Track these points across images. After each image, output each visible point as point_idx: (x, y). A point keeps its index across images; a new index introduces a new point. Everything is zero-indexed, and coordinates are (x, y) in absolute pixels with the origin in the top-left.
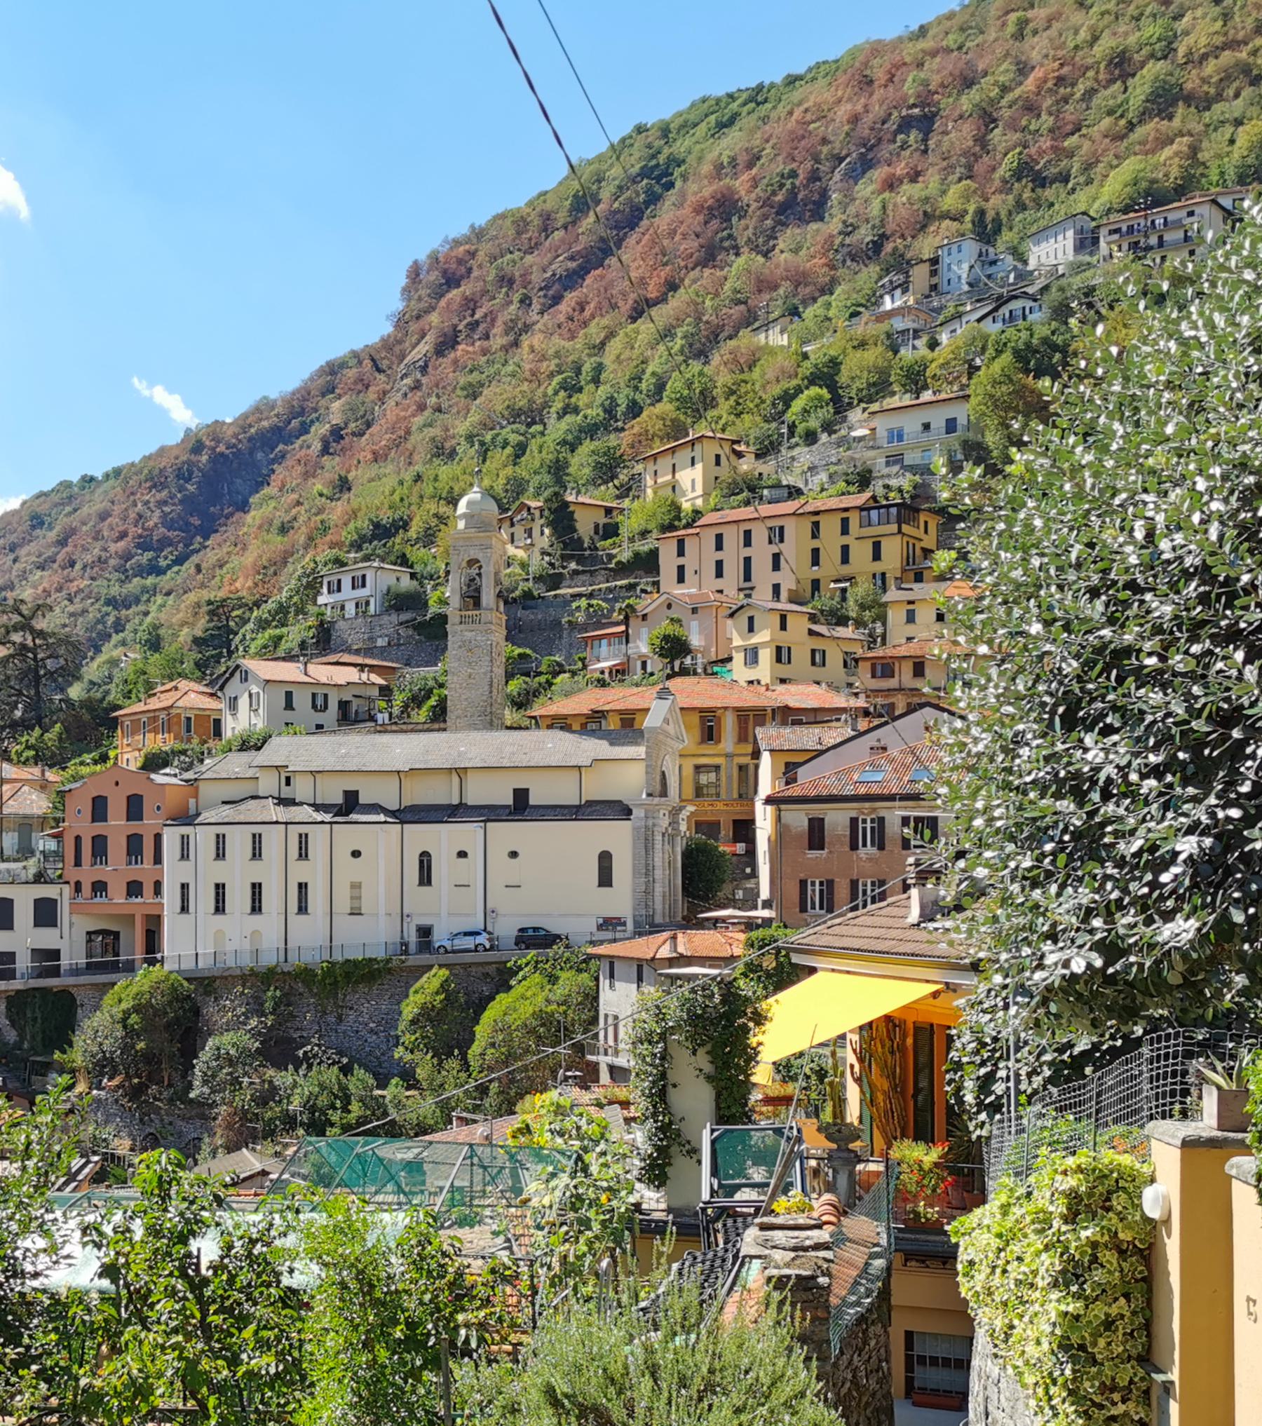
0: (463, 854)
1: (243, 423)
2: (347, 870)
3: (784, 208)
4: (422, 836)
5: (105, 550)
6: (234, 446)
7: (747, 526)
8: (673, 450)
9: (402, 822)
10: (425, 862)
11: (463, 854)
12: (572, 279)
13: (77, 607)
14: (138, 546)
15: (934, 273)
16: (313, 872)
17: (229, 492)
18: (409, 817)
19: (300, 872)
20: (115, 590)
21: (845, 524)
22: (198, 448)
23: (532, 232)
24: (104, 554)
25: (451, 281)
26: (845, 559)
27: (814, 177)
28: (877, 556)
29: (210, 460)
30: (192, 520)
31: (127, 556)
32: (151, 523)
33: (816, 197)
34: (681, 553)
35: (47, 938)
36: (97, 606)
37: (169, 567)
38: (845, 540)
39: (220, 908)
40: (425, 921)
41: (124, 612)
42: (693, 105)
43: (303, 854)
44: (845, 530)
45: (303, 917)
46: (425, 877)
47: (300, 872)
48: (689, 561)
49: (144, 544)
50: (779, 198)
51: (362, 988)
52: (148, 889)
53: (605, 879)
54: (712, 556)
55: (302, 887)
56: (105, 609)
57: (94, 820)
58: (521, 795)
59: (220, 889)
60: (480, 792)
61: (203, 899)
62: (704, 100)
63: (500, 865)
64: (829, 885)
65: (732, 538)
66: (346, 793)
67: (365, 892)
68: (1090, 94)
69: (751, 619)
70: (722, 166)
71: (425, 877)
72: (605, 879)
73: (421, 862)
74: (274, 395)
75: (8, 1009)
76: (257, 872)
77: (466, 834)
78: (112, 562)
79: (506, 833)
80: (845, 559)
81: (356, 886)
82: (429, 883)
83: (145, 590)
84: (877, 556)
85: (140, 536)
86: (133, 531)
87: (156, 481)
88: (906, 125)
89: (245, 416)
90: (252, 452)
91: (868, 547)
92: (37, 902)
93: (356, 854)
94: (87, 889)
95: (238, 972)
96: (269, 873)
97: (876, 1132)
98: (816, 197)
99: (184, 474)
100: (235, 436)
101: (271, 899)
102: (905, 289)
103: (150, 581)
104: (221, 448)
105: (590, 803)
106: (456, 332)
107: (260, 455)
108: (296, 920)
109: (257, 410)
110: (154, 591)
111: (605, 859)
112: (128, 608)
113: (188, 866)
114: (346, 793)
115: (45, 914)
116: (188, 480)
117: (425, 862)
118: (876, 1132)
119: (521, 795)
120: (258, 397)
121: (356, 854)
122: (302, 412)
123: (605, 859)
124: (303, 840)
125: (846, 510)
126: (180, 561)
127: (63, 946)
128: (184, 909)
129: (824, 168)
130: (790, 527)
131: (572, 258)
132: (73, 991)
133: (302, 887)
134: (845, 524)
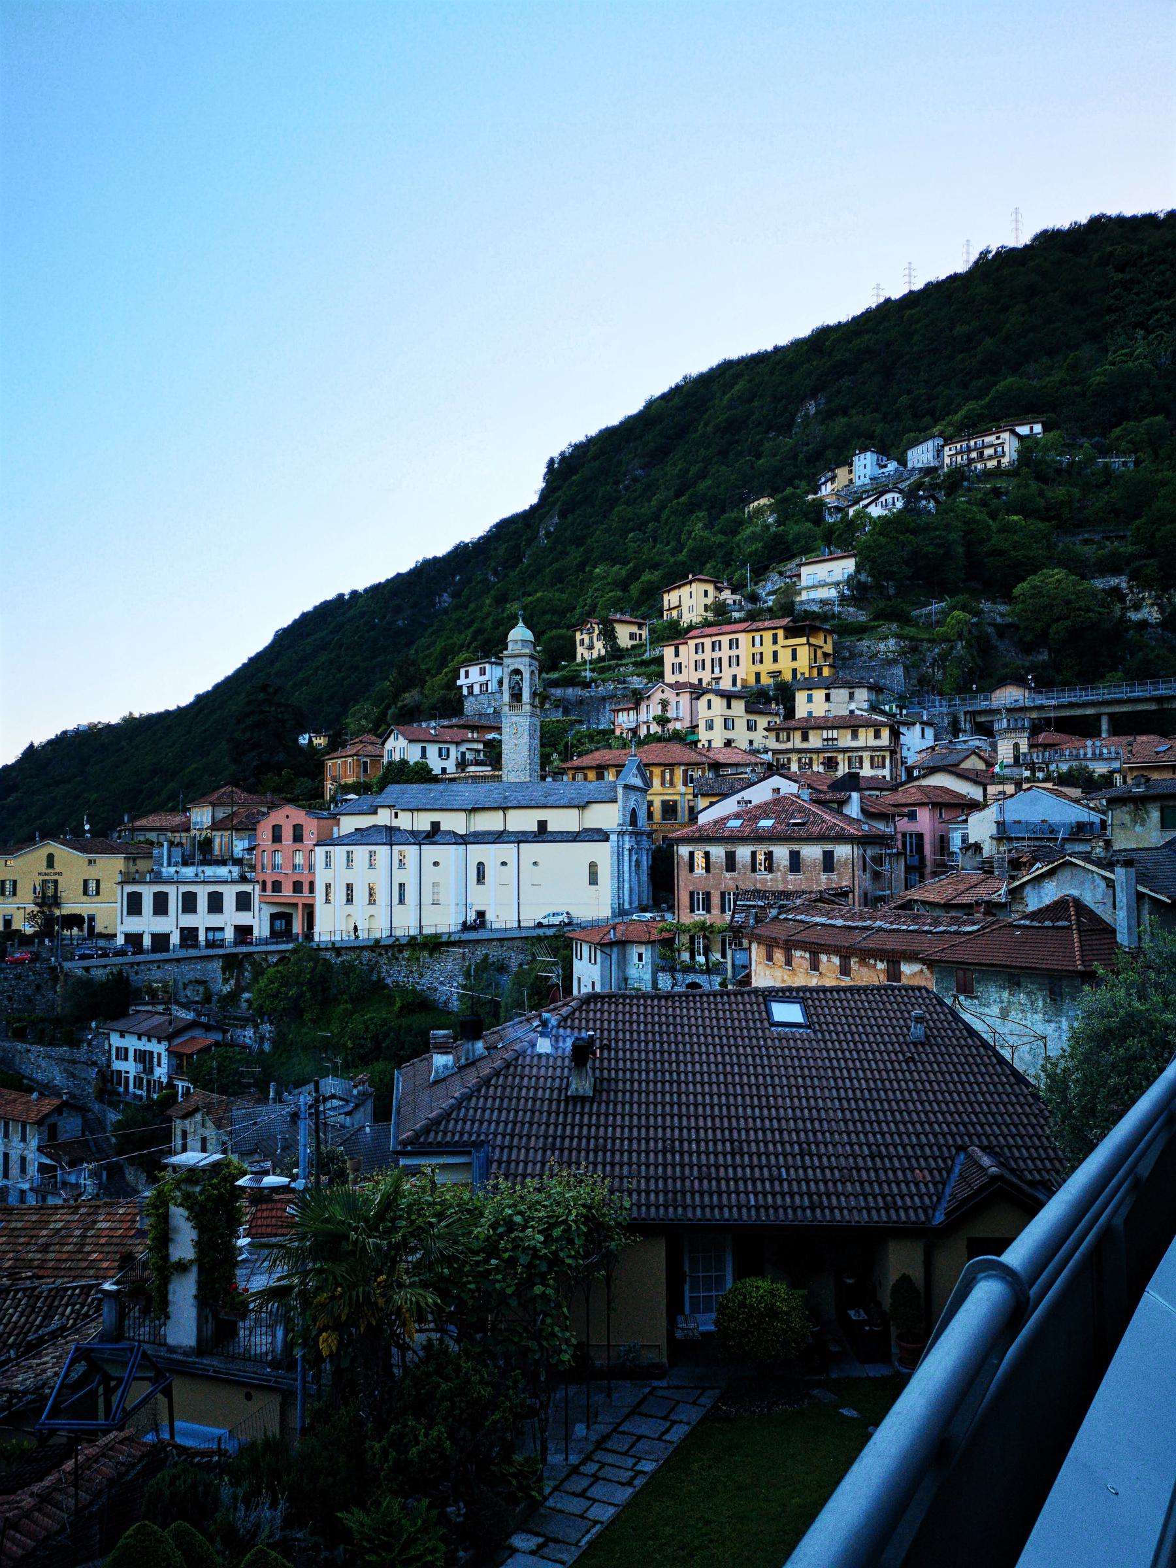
0: (504, 864)
4: (477, 852)
10: (481, 867)
11: (504, 864)
16: (408, 876)
18: (471, 839)
21: (775, 637)
26: (775, 660)
28: (794, 658)
34: (677, 655)
35: (244, 918)
38: (775, 648)
39: (349, 900)
40: (481, 908)
44: (775, 642)
46: (481, 878)
52: (306, 888)
53: (593, 880)
55: (402, 886)
57: (274, 841)
59: (349, 887)
61: (339, 894)
64: (707, 895)
66: (432, 823)
67: (441, 889)
69: (709, 701)
71: (481, 878)
72: (593, 880)
73: (478, 869)
74: (467, 540)
77: (507, 851)
79: (530, 850)
80: (775, 660)
81: (435, 885)
82: (483, 883)
84: (794, 658)
91: (789, 650)
92: (238, 894)
93: (436, 864)
94: (269, 886)
97: (114, 1409)
101: (382, 896)
105: (586, 830)
108: (397, 908)
111: (593, 866)
113: (330, 872)
114: (432, 823)
115: (243, 902)
117: (481, 867)
118: (114, 1409)
121: (436, 864)
123: (593, 866)
127: (255, 923)
128: (327, 901)
133: (402, 886)
134: (775, 637)
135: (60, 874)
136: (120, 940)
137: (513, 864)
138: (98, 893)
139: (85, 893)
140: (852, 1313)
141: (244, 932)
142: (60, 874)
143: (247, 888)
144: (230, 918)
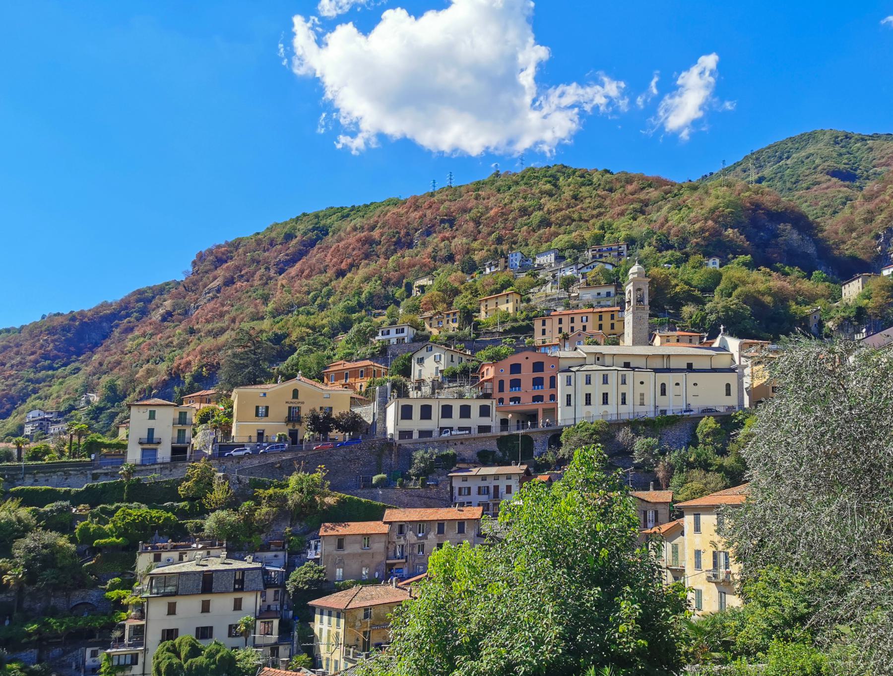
1: (96, 311)
2: (640, 389)
3: (396, 243)
5: (24, 359)
6: (92, 319)
7: (572, 316)
8: (497, 298)
9: (656, 372)
10: (663, 385)
11: (677, 384)
12: (293, 260)
13: (10, 382)
14: (42, 358)
15: (506, 262)
16: (627, 389)
17: (89, 338)
19: (623, 388)
20: (32, 376)
22: (73, 319)
23: (265, 244)
24: (23, 361)
25: (220, 261)
27: (408, 234)
29: (79, 324)
30: (71, 348)
31: (37, 362)
32: (49, 349)
33: (409, 241)
34: (544, 324)
35: (485, 421)
36: (22, 382)
37: (59, 368)
38: (613, 321)
41: (37, 385)
42: (327, 209)
43: (624, 383)
45: (624, 406)
46: (663, 393)
47: (623, 388)
48: (548, 327)
49: (45, 357)
50: (394, 240)
51: (668, 427)
53: (728, 393)
54: (557, 326)
56: (27, 384)
58: (690, 366)
60: (674, 364)
62: (332, 208)
63: (692, 390)
65: (566, 320)
68: (515, 219)
70: (357, 228)
71: (663, 393)
72: (728, 393)
75: (498, 444)
76: (605, 389)
78: (28, 364)
81: (642, 395)
83: (48, 376)
85: (43, 354)
86: (39, 352)
87: (51, 331)
88: (443, 221)
89: (97, 308)
90: (101, 322)
93: (642, 383)
95: (622, 422)
96: (612, 389)
98: (409, 241)
99: (65, 329)
100: (92, 315)
102: (496, 266)
103: (50, 372)
104: (86, 320)
105: (712, 369)
106: (233, 278)
107: (104, 324)
109: (102, 306)
110: (53, 376)
111: (728, 386)
112: (40, 383)
115: (485, 411)
116: (68, 332)
117: (663, 385)
119: (690, 366)
120: (103, 301)
122: (126, 308)
123: (728, 386)
124: (624, 377)
125: (613, 311)
126: (65, 365)
129: (411, 232)
130: (590, 316)
131: (287, 255)
132: (531, 435)
135: (303, 403)
136: (416, 436)
137: (683, 384)
138: (267, 415)
139: (257, 415)
140: (329, 483)
141: (483, 429)
142: (303, 403)
143: (487, 402)
144: (475, 420)
